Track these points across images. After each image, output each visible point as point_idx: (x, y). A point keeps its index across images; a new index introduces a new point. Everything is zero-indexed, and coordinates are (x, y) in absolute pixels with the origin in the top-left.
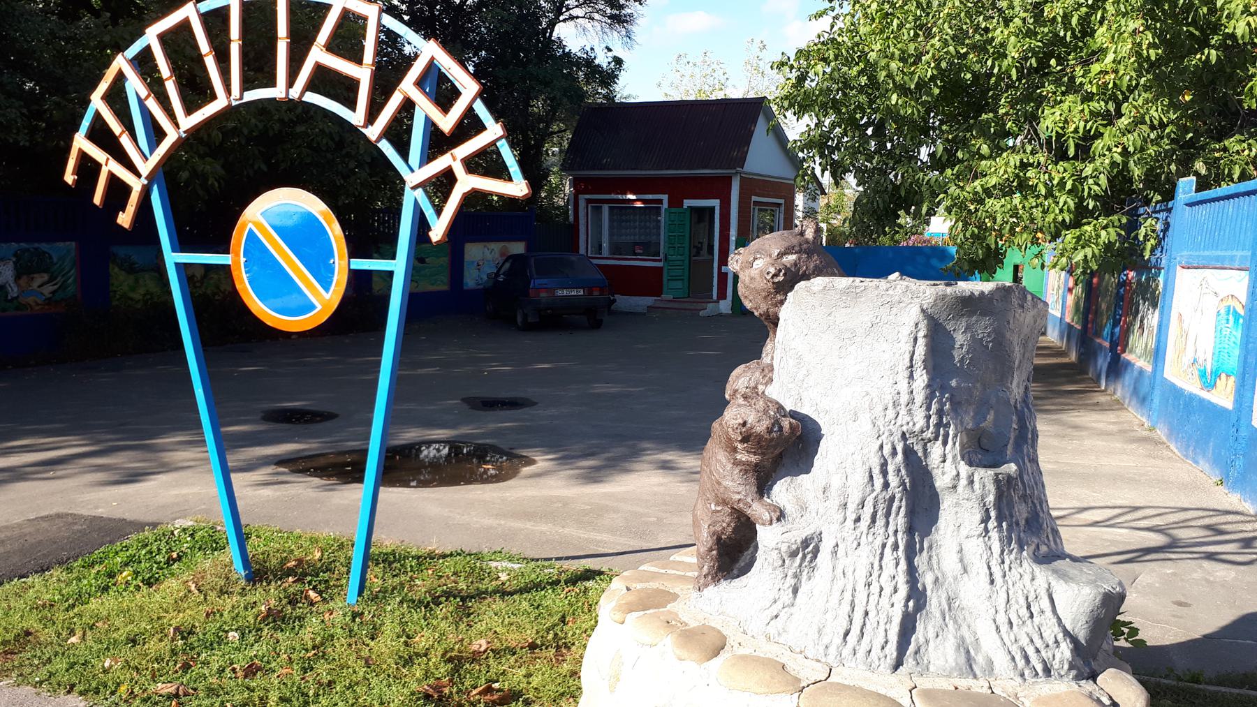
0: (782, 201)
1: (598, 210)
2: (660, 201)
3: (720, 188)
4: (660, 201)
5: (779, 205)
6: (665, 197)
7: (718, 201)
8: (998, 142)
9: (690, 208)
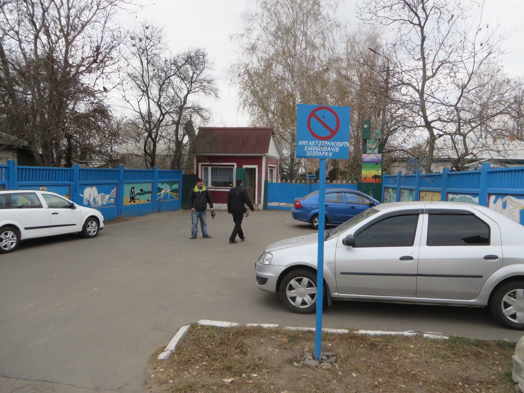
0: (275, 166)
1: (206, 170)
2: (233, 166)
3: (257, 160)
4: (233, 166)
5: (274, 167)
6: (235, 164)
7: (257, 166)
8: (75, 33)
9: (246, 169)
